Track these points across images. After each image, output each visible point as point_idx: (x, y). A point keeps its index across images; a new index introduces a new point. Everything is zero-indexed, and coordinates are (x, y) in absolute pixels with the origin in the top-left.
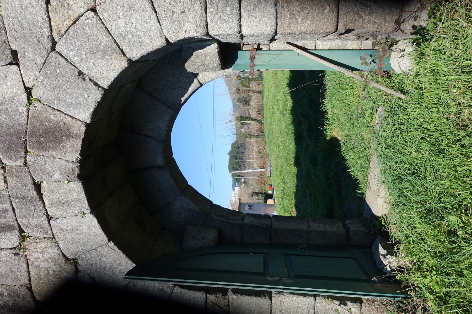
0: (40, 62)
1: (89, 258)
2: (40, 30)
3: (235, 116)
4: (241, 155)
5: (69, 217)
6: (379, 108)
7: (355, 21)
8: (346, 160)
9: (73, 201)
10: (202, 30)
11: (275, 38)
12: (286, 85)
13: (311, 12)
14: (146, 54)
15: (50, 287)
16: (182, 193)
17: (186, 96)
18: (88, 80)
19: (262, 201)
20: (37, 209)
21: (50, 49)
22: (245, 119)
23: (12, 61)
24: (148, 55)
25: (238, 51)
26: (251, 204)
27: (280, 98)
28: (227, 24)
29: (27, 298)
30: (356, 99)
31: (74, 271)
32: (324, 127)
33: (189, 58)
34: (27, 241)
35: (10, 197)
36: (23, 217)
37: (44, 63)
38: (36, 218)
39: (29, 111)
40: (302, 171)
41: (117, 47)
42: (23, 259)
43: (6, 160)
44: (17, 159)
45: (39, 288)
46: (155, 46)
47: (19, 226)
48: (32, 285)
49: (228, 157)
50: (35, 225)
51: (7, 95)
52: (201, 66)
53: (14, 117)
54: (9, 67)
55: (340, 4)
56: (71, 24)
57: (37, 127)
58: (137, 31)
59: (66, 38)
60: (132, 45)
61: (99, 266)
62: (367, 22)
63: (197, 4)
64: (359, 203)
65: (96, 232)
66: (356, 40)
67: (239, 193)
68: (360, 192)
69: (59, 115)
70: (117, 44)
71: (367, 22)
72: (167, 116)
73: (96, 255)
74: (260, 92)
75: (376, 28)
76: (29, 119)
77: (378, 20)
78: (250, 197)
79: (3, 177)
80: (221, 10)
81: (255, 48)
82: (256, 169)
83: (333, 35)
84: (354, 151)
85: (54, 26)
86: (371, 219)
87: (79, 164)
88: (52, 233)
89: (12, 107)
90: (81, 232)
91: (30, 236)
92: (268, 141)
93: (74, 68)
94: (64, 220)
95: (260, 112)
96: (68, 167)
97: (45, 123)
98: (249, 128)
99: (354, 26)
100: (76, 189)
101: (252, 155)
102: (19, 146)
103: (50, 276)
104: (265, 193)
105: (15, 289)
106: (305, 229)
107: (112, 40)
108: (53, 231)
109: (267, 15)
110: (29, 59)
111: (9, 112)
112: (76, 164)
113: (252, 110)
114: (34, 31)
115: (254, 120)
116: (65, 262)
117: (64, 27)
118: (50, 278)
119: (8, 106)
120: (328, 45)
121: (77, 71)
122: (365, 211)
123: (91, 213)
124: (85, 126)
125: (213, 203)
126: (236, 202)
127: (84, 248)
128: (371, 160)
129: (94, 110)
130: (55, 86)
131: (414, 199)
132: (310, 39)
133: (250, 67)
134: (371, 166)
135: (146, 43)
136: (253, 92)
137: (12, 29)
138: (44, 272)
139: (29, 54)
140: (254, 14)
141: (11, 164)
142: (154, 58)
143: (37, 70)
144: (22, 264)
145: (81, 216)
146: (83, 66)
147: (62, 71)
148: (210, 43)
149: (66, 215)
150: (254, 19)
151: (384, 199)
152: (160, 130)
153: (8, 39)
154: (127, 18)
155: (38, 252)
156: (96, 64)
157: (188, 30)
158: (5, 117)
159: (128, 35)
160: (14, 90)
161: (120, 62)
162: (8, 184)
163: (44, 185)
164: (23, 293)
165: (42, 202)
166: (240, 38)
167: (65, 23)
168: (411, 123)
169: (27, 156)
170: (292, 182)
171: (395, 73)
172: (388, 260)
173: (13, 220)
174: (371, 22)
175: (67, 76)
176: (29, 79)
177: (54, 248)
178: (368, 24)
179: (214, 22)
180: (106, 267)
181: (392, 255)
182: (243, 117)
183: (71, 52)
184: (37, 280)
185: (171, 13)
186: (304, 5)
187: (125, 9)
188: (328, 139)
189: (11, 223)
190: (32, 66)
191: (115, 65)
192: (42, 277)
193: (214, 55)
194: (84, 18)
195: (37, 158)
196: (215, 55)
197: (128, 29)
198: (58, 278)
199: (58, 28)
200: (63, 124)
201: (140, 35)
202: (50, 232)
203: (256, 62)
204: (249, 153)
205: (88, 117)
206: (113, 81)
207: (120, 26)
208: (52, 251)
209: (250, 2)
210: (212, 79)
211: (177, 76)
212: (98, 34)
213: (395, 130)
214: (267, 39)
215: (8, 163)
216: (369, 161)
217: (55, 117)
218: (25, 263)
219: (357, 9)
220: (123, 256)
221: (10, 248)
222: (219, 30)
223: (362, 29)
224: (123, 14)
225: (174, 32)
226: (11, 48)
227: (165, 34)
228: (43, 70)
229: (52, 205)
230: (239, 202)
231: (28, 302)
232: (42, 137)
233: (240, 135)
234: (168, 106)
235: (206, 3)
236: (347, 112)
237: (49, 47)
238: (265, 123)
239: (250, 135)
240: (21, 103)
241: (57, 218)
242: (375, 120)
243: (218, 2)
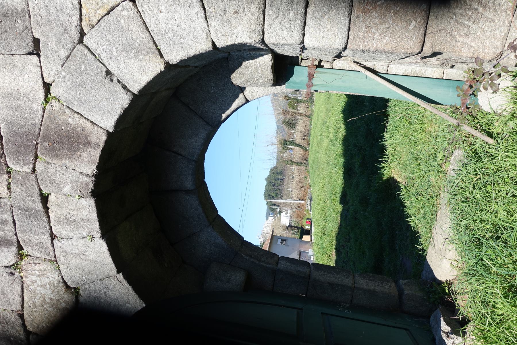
0: (63, 55)
1: (93, 290)
2: (68, 18)
3: (278, 139)
4: (279, 183)
5: (76, 239)
6: (456, 150)
7: (446, 43)
8: (405, 207)
9: (83, 220)
10: (257, 35)
11: (341, 55)
12: (341, 111)
13: (392, 26)
14: (187, 58)
15: (45, 317)
16: (210, 224)
17: (228, 112)
18: (117, 82)
19: (297, 236)
20: (41, 225)
21: (76, 41)
22: (288, 143)
23: (32, 51)
24: (190, 59)
25: (295, 66)
26: (285, 239)
27: (331, 124)
28: (287, 31)
29: (17, 326)
30: (426, 136)
31: (74, 301)
32: (382, 164)
33: (237, 69)
34: (25, 261)
35: (12, 208)
36: (24, 232)
37: (68, 57)
38: (38, 235)
39: (45, 110)
40: (348, 211)
41: (155, 47)
42: (18, 280)
43: (13, 163)
44: (24, 164)
45: (31, 317)
46: (199, 49)
47: (18, 242)
48: (25, 312)
49: (265, 183)
50: (36, 243)
51: (22, 89)
52: (250, 79)
53: (27, 115)
54: (28, 57)
55: (429, 20)
56: (104, 14)
57: (52, 130)
58: (180, 29)
59: (97, 30)
60: (172, 45)
61: (103, 301)
62: (461, 46)
63: (254, 4)
64: (416, 260)
65: (105, 260)
66: (440, 67)
67: (272, 224)
68: (420, 247)
69: (78, 119)
70: (155, 43)
71: (461, 46)
72: (203, 133)
73: (102, 287)
74: (308, 116)
75: (471, 54)
76: (44, 120)
77: (476, 44)
78: (284, 230)
79: (7, 183)
80: (282, 13)
81: (315, 65)
82: (295, 200)
83: (414, 57)
84: (417, 198)
85: (84, 15)
86: (432, 283)
87: (94, 179)
88: (54, 255)
89: (26, 103)
90: (88, 258)
91: (29, 255)
92: (311, 171)
93: (102, 66)
94: (70, 241)
95: (305, 138)
96: (81, 180)
97: (61, 127)
98: (291, 154)
99: (444, 49)
100: (88, 207)
101: (292, 183)
102: (29, 149)
103: (46, 304)
104: (301, 227)
105: (5, 314)
106: (350, 284)
107: (149, 37)
108: (56, 253)
109: (337, 24)
110: (52, 50)
111: (23, 109)
112: (91, 179)
113: (297, 134)
114: (62, 18)
115: (299, 146)
116: (65, 291)
117: (96, 17)
118: (45, 306)
119: (22, 102)
120: (404, 69)
121: (105, 69)
122: (424, 272)
123: (101, 237)
124: (106, 134)
125: (245, 239)
126: (267, 233)
127: (89, 278)
128: (439, 212)
129: (119, 118)
130: (77, 84)
131: (494, 269)
132: (383, 60)
133: (307, 86)
134: (437, 218)
135: (189, 45)
136: (301, 115)
137: (37, 13)
138: (39, 299)
139: (53, 45)
140: (322, 23)
141: (18, 169)
142: (196, 64)
143: (59, 63)
144: (16, 286)
145: (89, 239)
146: (112, 64)
147: (88, 68)
148: (263, 53)
149: (72, 236)
150: (321, 28)
151: (451, 261)
152: (193, 149)
153: (31, 24)
154: (170, 13)
155: (36, 275)
156: (128, 64)
157: (239, 34)
158: (17, 114)
159: (169, 34)
160: (31, 85)
161: (155, 64)
162: (11, 192)
163: (51, 198)
164: (13, 320)
165: (47, 217)
166: (300, 51)
167: (98, 12)
168: (499, 175)
169: (37, 162)
170: (335, 221)
171: (481, 111)
172: (452, 340)
173: (12, 234)
174: (466, 46)
175: (93, 74)
176: (49, 73)
177: (54, 273)
178: (462, 47)
179: (272, 28)
180: (111, 303)
181: (458, 335)
182: (286, 141)
183: (101, 47)
184: (30, 306)
185: (222, 12)
186: (384, 17)
187: (169, 2)
188: (385, 178)
189: (9, 238)
190: (54, 59)
191: (150, 67)
192: (37, 305)
193: (266, 68)
194: (120, 8)
195: (47, 166)
196: (268, 68)
197: (170, 26)
198: (55, 308)
199: (89, 17)
200: (82, 129)
201: (183, 35)
202: (52, 254)
203: (315, 81)
204: (288, 181)
205: (111, 125)
206: (145, 86)
207: (160, 22)
208: (52, 276)
209: (318, 7)
210: (261, 96)
211: (220, 88)
212: (133, 30)
213: (477, 180)
214: (332, 55)
215: (14, 168)
216: (436, 212)
217: (74, 121)
218: (20, 286)
219: (450, 28)
220: (132, 292)
221: (5, 266)
222: (277, 37)
223: (453, 53)
224: (166, 8)
225: (223, 35)
226: (33, 36)
227: (212, 37)
228: (66, 65)
229: (58, 222)
230: (271, 234)
231: (17, 331)
232: (55, 142)
233: (280, 159)
234: (206, 122)
235: (265, 4)
236: (412, 150)
237: (76, 38)
238: (310, 150)
239: (292, 162)
240: (37, 100)
241: (62, 239)
242: (449, 164)
243: (280, 5)
